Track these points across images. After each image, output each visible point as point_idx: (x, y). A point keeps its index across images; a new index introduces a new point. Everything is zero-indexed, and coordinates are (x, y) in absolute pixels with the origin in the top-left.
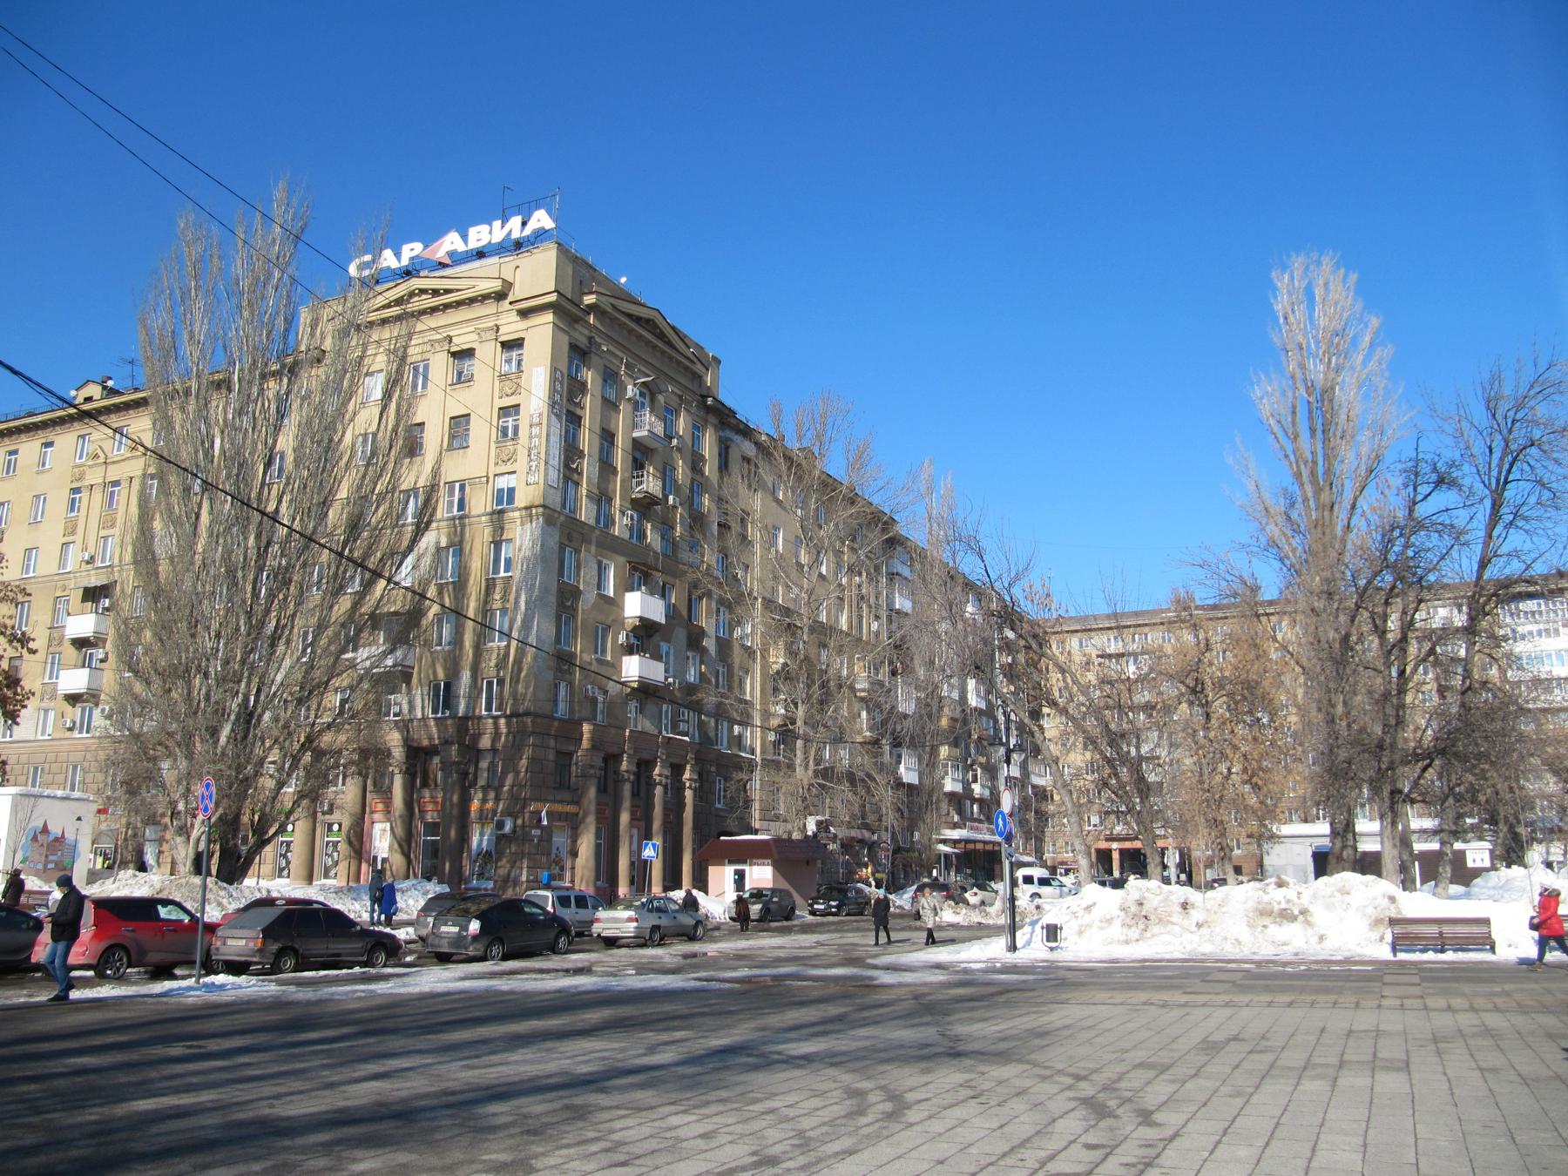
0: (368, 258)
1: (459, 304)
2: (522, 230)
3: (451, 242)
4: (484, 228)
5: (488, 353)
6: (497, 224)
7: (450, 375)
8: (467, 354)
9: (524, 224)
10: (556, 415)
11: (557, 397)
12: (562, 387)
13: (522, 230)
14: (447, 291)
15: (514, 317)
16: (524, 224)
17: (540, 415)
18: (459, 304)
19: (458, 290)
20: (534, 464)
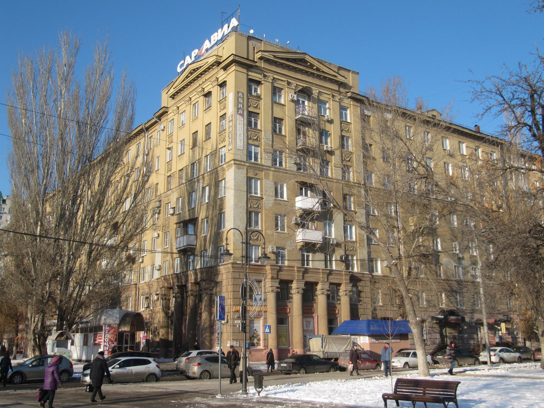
0: (182, 62)
1: (205, 71)
2: (210, 43)
3: (207, 44)
4: (216, 34)
5: (216, 91)
6: (220, 30)
7: (205, 106)
8: (208, 95)
9: (191, 57)
10: (240, 114)
11: (240, 106)
12: (243, 100)
13: (210, 43)
14: (198, 69)
15: (222, 72)
16: (191, 57)
17: (232, 115)
18: (205, 71)
19: (200, 67)
20: (230, 140)
